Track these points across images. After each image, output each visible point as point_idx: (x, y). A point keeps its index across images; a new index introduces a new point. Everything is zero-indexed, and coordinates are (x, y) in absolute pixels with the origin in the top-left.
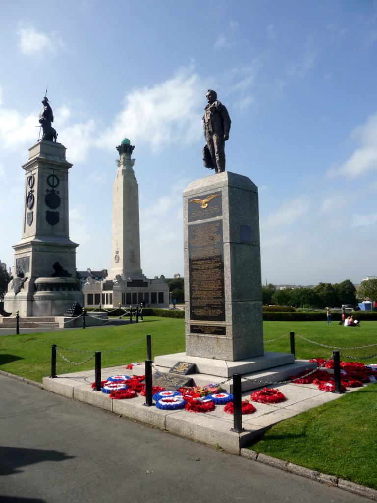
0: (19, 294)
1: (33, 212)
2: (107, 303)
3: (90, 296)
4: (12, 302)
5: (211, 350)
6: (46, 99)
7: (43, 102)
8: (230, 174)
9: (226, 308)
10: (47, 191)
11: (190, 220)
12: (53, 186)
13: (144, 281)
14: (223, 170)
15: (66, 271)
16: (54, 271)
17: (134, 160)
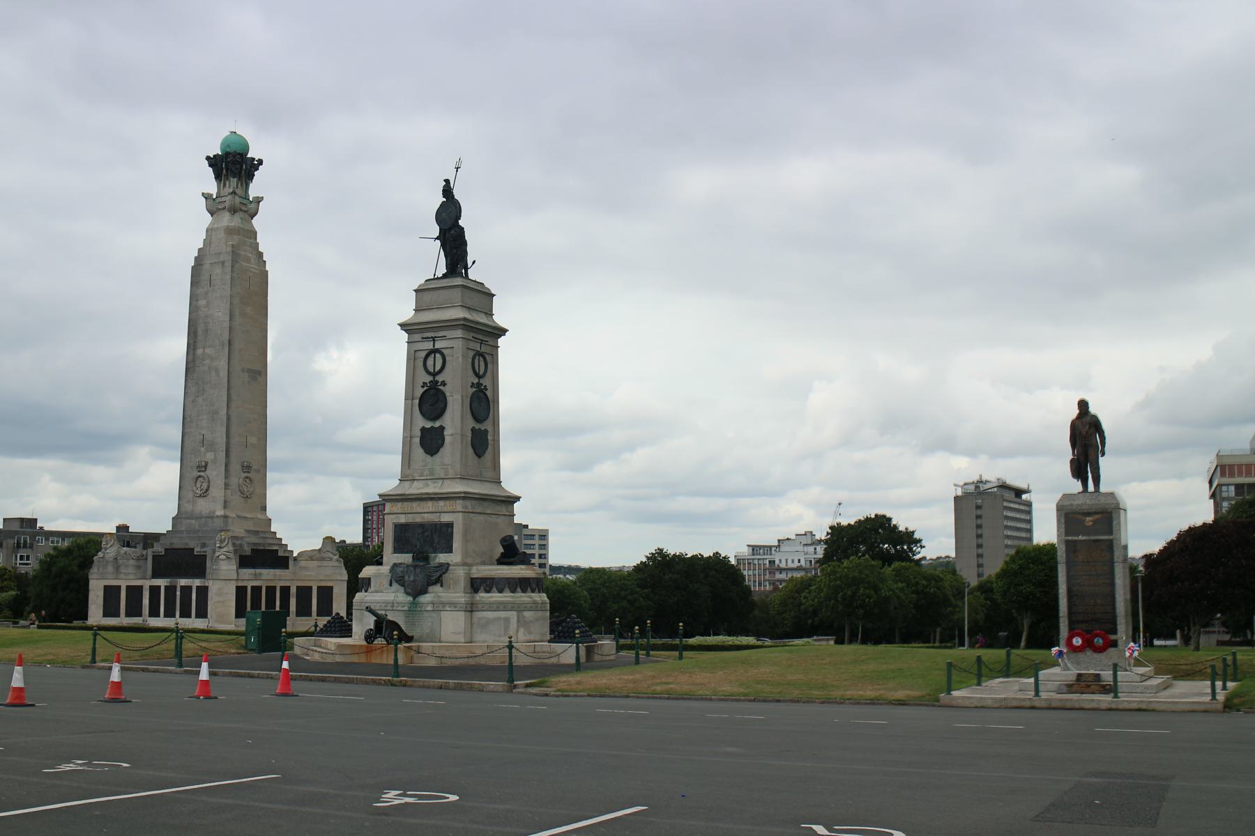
1: (442, 428)
3: (111, 594)
11: (1067, 534)
13: (280, 554)
17: (258, 200)
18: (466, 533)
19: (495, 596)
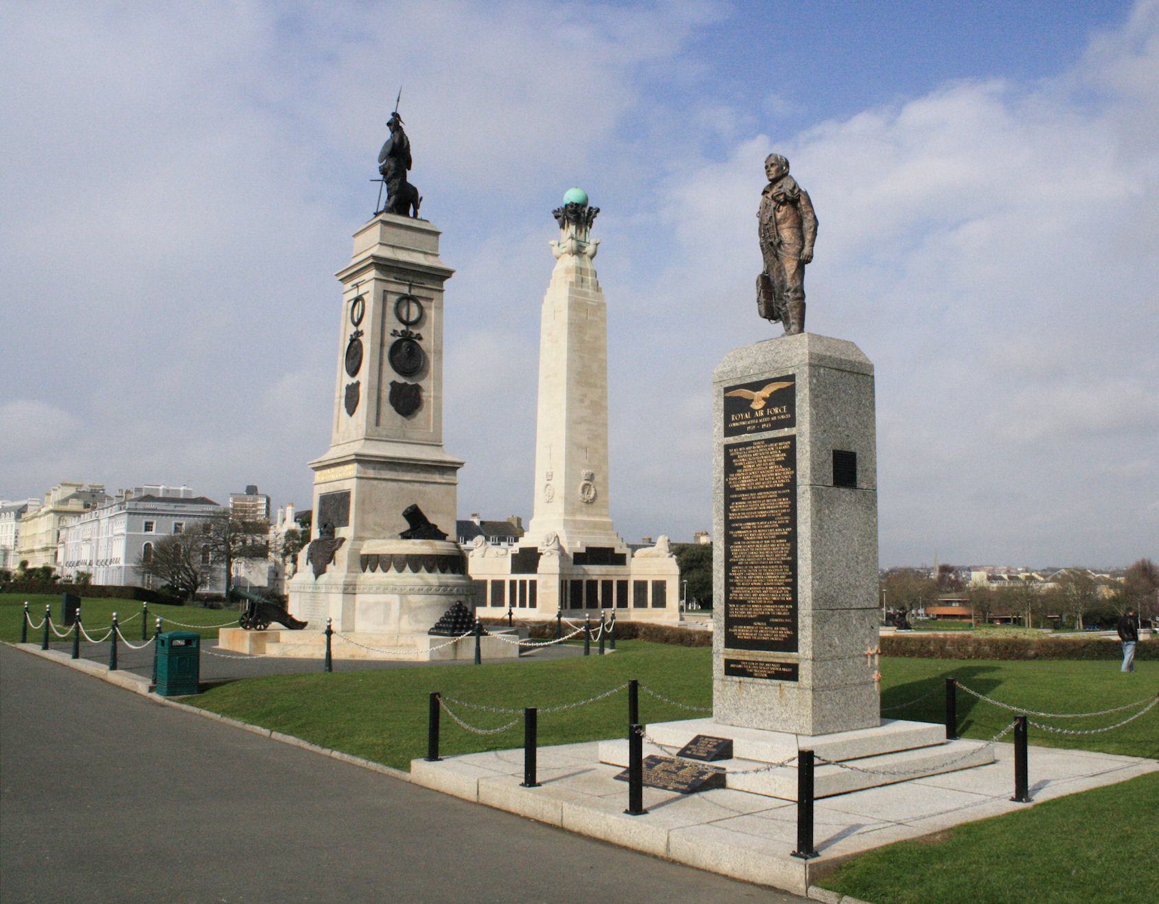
0: (323, 578)
1: (358, 384)
2: (523, 605)
4: (308, 596)
5: (767, 712)
6: (396, 116)
7: (388, 124)
8: (812, 336)
9: (800, 625)
10: (395, 333)
12: (407, 323)
14: (801, 330)
15: (435, 526)
16: (405, 526)
18: (361, 503)
19: (379, 575)
